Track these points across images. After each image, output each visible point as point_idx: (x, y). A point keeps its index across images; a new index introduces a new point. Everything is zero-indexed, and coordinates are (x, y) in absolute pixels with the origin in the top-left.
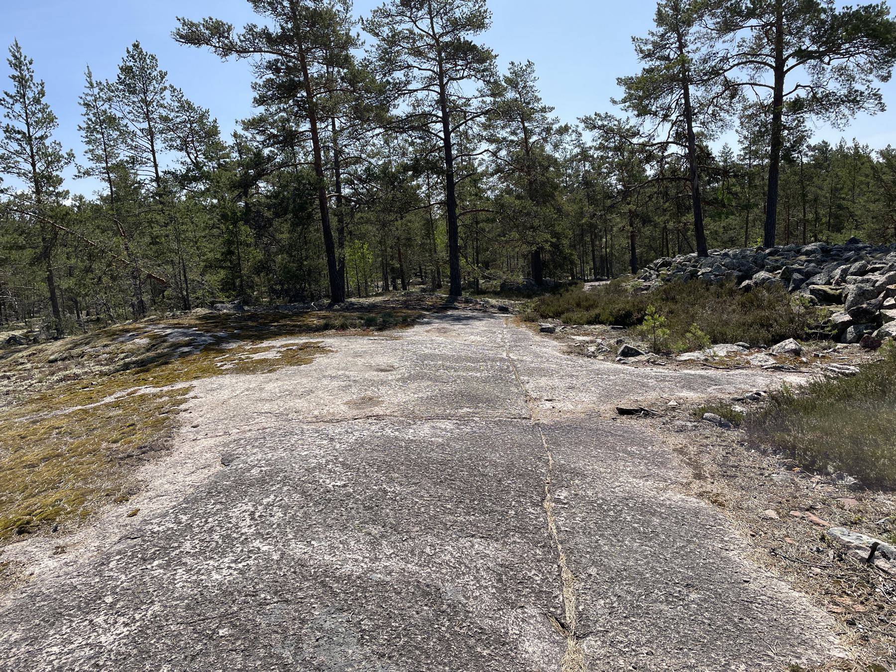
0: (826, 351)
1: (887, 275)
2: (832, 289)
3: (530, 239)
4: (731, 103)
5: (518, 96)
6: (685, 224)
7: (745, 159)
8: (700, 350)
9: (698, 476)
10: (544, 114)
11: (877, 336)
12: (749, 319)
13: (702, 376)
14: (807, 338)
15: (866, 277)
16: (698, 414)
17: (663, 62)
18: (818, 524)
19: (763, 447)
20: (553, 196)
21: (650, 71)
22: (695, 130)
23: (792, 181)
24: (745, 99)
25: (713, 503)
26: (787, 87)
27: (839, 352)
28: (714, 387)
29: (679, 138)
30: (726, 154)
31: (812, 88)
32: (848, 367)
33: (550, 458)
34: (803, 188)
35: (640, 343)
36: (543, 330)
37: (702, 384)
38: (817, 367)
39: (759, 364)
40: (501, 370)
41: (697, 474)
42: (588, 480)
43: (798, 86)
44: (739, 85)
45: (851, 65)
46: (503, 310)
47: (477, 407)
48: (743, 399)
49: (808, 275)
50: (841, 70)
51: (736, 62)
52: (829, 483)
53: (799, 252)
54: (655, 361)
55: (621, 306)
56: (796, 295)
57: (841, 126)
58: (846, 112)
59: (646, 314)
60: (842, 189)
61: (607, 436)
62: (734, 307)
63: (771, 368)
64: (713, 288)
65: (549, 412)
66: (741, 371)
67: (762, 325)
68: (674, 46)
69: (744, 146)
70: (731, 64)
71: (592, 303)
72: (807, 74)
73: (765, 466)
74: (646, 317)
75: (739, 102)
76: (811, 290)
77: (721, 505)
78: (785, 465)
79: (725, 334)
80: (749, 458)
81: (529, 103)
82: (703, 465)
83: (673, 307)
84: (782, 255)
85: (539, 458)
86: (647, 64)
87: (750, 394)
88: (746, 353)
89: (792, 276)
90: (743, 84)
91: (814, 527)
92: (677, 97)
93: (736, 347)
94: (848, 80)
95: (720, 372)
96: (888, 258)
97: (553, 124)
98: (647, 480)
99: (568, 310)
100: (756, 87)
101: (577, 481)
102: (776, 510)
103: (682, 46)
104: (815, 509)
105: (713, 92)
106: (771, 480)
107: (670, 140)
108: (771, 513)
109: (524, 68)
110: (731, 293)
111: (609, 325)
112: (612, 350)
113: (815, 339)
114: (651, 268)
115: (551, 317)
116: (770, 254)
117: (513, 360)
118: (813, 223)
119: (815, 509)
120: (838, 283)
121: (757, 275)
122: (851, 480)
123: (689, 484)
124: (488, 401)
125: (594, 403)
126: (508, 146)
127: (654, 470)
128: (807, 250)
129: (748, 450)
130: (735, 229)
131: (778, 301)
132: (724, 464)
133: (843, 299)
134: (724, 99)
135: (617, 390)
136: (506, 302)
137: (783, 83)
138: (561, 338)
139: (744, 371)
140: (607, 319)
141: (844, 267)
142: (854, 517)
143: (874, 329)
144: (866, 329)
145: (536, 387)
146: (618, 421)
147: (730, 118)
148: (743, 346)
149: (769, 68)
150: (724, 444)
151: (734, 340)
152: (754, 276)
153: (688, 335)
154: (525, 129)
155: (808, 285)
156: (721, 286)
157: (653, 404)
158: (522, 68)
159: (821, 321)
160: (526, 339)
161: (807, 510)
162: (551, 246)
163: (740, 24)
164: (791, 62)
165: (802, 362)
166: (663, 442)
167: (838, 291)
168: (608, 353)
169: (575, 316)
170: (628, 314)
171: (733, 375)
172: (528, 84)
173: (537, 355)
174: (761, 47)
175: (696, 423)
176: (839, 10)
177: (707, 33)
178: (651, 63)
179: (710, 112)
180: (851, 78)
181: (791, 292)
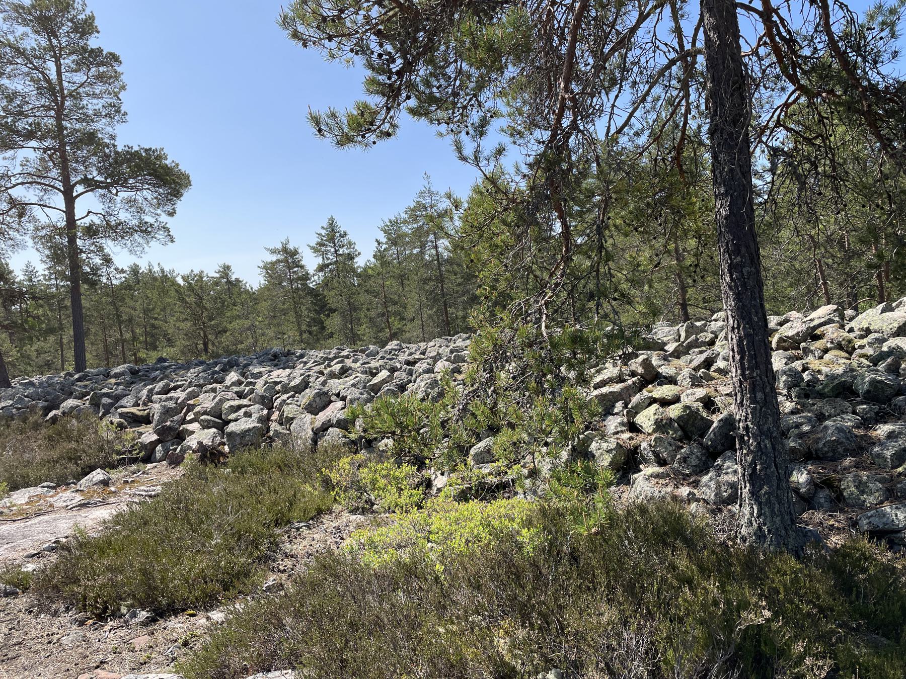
0: (135, 475)
1: (187, 392)
7: (50, 279)
11: (180, 451)
12: (55, 454)
14: (112, 466)
15: (169, 395)
23: (104, 302)
24: (36, 220)
26: (79, 211)
27: (148, 474)
28: (6, 546)
30: (30, 273)
31: (104, 216)
32: (154, 488)
38: (126, 494)
39: (65, 504)
43: (89, 212)
45: (140, 199)
48: (38, 554)
49: (118, 398)
50: (130, 202)
51: (20, 181)
52: (122, 627)
53: (108, 376)
56: (104, 422)
57: (138, 253)
58: (140, 240)
60: (153, 309)
62: (40, 442)
63: (77, 506)
64: (15, 424)
67: (70, 459)
70: (13, 182)
72: (98, 202)
73: (54, 630)
75: (30, 222)
79: (28, 476)
84: (90, 380)
87: (47, 545)
88: (51, 494)
89: (100, 400)
90: (485, 175)
93: (39, 489)
94: (138, 212)
96: (189, 375)
100: (46, 209)
104: (105, 663)
110: (36, 427)
113: (123, 464)
116: (79, 380)
118: (131, 342)
120: (145, 404)
121: (64, 404)
122: (143, 615)
128: (115, 373)
129: (37, 616)
130: (49, 352)
134: (12, 217)
137: (74, 208)
139: (46, 517)
141: (149, 387)
143: (178, 444)
147: (21, 238)
148: (48, 487)
150: (8, 618)
151: (38, 481)
152: (62, 406)
155: (117, 408)
156: (25, 421)
159: (128, 445)
161: (98, 667)
163: (20, 143)
164: (79, 189)
167: (146, 412)
171: (30, 526)
174: (47, 169)
180: (141, 210)
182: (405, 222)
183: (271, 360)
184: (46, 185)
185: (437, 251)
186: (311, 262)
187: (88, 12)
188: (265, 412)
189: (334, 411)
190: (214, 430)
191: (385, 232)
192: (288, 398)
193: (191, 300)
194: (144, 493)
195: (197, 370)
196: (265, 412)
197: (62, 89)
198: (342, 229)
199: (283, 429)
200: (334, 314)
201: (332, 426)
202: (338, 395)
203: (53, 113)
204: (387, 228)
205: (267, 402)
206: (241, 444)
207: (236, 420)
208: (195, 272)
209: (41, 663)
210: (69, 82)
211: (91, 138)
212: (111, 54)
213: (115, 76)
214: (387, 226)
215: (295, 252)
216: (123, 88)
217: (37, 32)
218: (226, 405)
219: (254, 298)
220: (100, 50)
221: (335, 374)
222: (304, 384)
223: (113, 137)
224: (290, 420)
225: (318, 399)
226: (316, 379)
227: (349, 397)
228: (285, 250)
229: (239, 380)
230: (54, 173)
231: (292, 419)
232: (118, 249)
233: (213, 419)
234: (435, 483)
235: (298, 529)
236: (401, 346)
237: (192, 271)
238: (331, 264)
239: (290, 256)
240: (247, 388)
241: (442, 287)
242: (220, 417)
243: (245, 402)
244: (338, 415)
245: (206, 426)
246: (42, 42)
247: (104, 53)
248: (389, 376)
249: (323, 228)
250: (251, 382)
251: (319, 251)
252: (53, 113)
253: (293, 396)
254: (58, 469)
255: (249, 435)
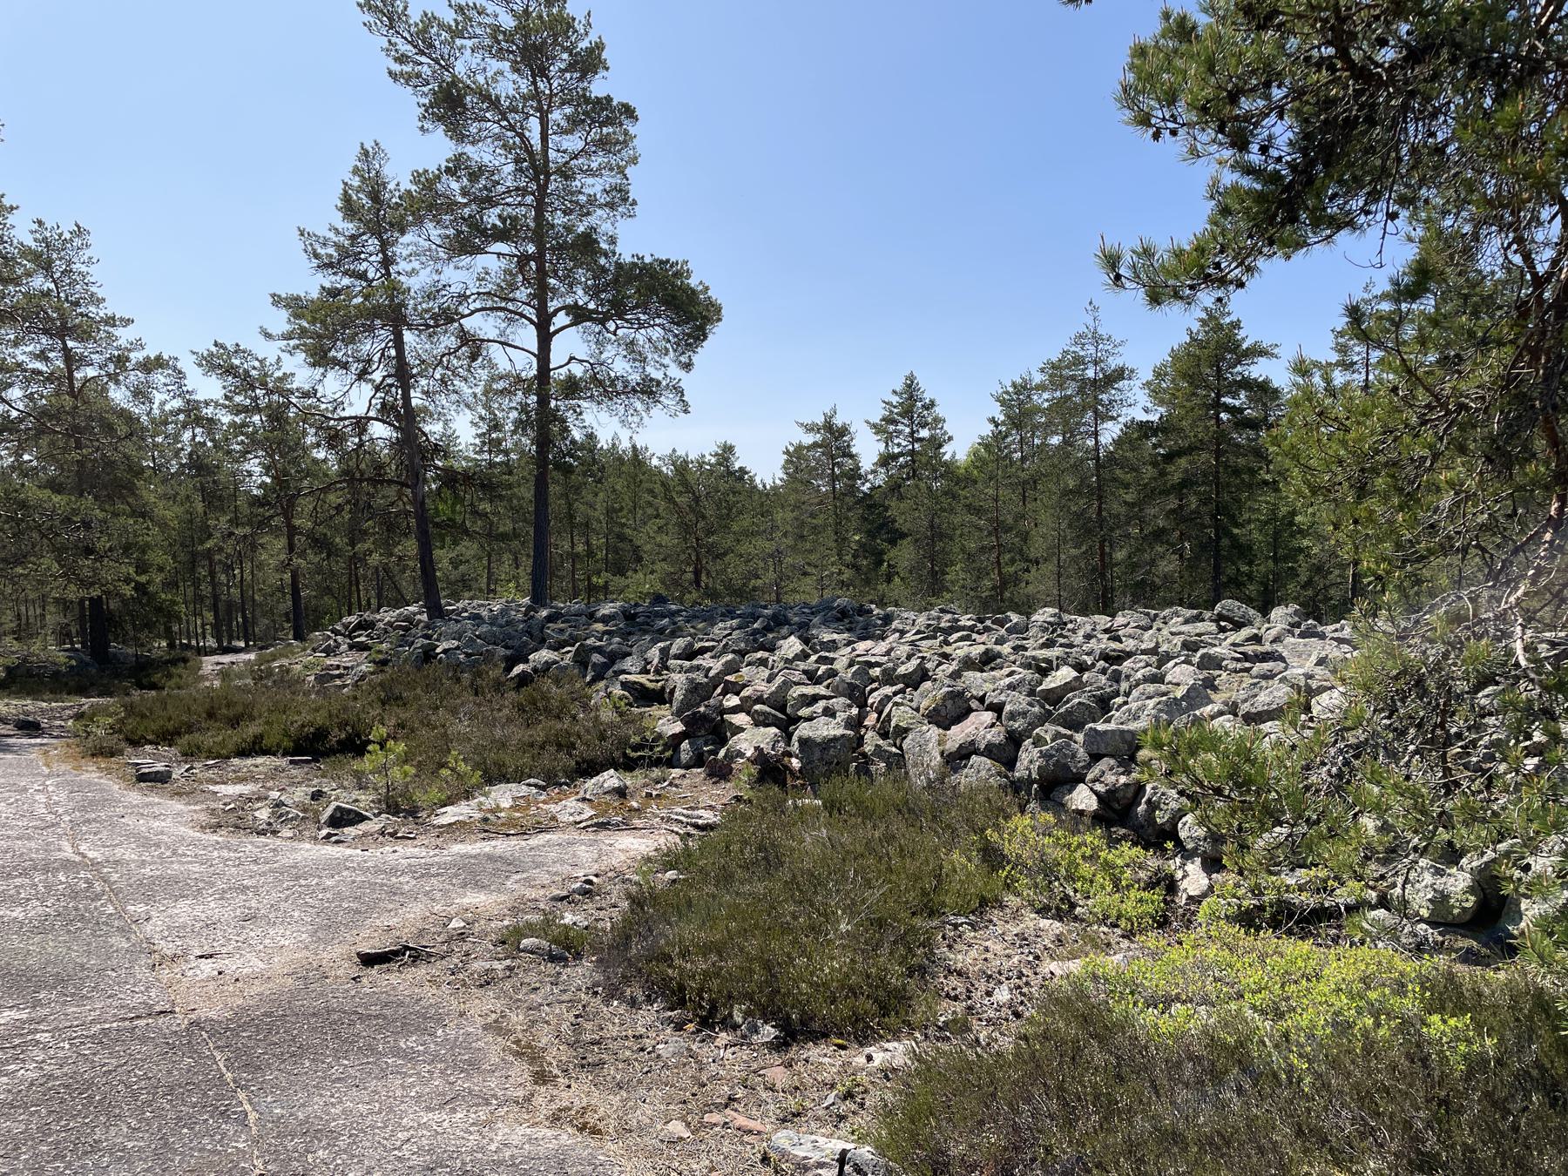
0: (659, 786)
2: (651, 681)
3: (87, 573)
4: (470, 366)
5: (52, 286)
6: (400, 558)
8: (467, 799)
9: (541, 1078)
10: (111, 330)
12: (538, 733)
13: (490, 858)
15: (695, 662)
16: (509, 941)
17: (357, 283)
18: (750, 1132)
19: (628, 991)
20: (132, 489)
21: (334, 293)
22: (414, 402)
24: (493, 366)
25: (581, 1129)
27: (676, 786)
28: (518, 877)
29: (386, 412)
33: (248, 1107)
34: (570, 505)
35: (356, 794)
36: (142, 778)
37: (495, 873)
39: (571, 819)
40: (75, 895)
41: (537, 1073)
42: (343, 1142)
43: (572, 358)
44: (483, 341)
46: (29, 727)
47: (36, 1004)
48: (568, 897)
49: (614, 657)
50: (631, 345)
51: (478, 305)
53: (592, 617)
54: (396, 832)
55: (305, 717)
58: (638, 405)
59: (370, 742)
61: (352, 1024)
65: (212, 986)
66: (548, 836)
68: (373, 258)
69: (479, 431)
71: (240, 709)
74: (370, 748)
76: (622, 683)
77: (595, 1131)
78: (672, 1022)
80: (614, 1018)
81: (77, 304)
82: (544, 1050)
83: (405, 715)
85: (222, 1113)
86: (329, 280)
87: (578, 885)
88: (543, 798)
90: (489, 341)
91: (746, 1138)
92: (383, 345)
95: (513, 841)
97: (130, 351)
98: (454, 1111)
99: (190, 729)
100: (507, 349)
101: (320, 1153)
102: (683, 1119)
103: (387, 262)
104: (735, 1100)
105: (443, 346)
106: (659, 1056)
107: (372, 414)
108: (677, 1128)
109: (67, 236)
111: (284, 755)
112: (308, 815)
114: (336, 633)
115: (151, 743)
116: (550, 619)
117: (94, 863)
119: (735, 1100)
120: (658, 672)
123: (528, 1099)
124: (60, 980)
125: (307, 947)
126: (28, 381)
127: (463, 1084)
131: (574, 700)
132: (577, 1041)
133: (666, 696)
134: (459, 358)
135: (349, 910)
136: (28, 706)
138: (188, 794)
140: (278, 746)
141: (661, 645)
142: (792, 1103)
144: (706, 745)
145: (169, 928)
146: (365, 980)
148: (536, 786)
149: (527, 322)
150: (565, 997)
152: (531, 657)
153: (445, 772)
154: (68, 355)
157: (421, 932)
158: (60, 235)
160: (108, 801)
162: (135, 589)
164: (561, 319)
165: (631, 810)
166: (462, 1014)
167: (660, 684)
168: (304, 820)
169: (209, 739)
170: (321, 734)
171: (538, 848)
172: (73, 266)
173: (144, 842)
174: (513, 287)
175: (508, 962)
176: (627, 258)
177: (430, 250)
178: (333, 278)
179: (437, 376)
181: (590, 684)
182: (1041, 387)
183: (839, 620)
184: (511, 312)
185: (1097, 442)
186: (867, 450)
187: (593, 37)
188: (855, 711)
189: (978, 727)
190: (774, 730)
191: (1003, 403)
192: (895, 694)
193: (683, 500)
194: (685, 820)
195: (728, 624)
196: (855, 711)
197: (547, 160)
198: (927, 397)
199: (890, 745)
200: (905, 542)
201: (977, 752)
202: (981, 700)
203: (529, 199)
204: (1007, 397)
205: (857, 695)
206: (821, 759)
207: (810, 719)
208: (678, 453)
209: (640, 1082)
210: (558, 151)
211: (587, 245)
212: (624, 105)
213: (625, 141)
214: (1007, 393)
215: (843, 431)
216: (634, 160)
217: (516, 70)
218: (796, 691)
219: (767, 500)
220: (609, 99)
221: (974, 663)
222: (920, 673)
223: (612, 240)
224: (902, 732)
225: (949, 703)
226: (938, 666)
227: (1008, 708)
228: (828, 426)
229: (803, 651)
230: (523, 293)
231: (907, 730)
232: (604, 416)
233: (773, 712)
234: (1183, 885)
235: (956, 926)
236: (1060, 617)
237: (674, 450)
238: (901, 454)
239: (834, 436)
240: (823, 668)
241: (1100, 507)
242: (782, 709)
243: (821, 690)
244: (989, 737)
245: (760, 721)
246: (523, 86)
247: (615, 103)
248: (1076, 679)
249: (895, 392)
250: (826, 658)
251: (885, 431)
252: (529, 199)
253: (902, 691)
254: (546, 761)
255: (835, 747)
